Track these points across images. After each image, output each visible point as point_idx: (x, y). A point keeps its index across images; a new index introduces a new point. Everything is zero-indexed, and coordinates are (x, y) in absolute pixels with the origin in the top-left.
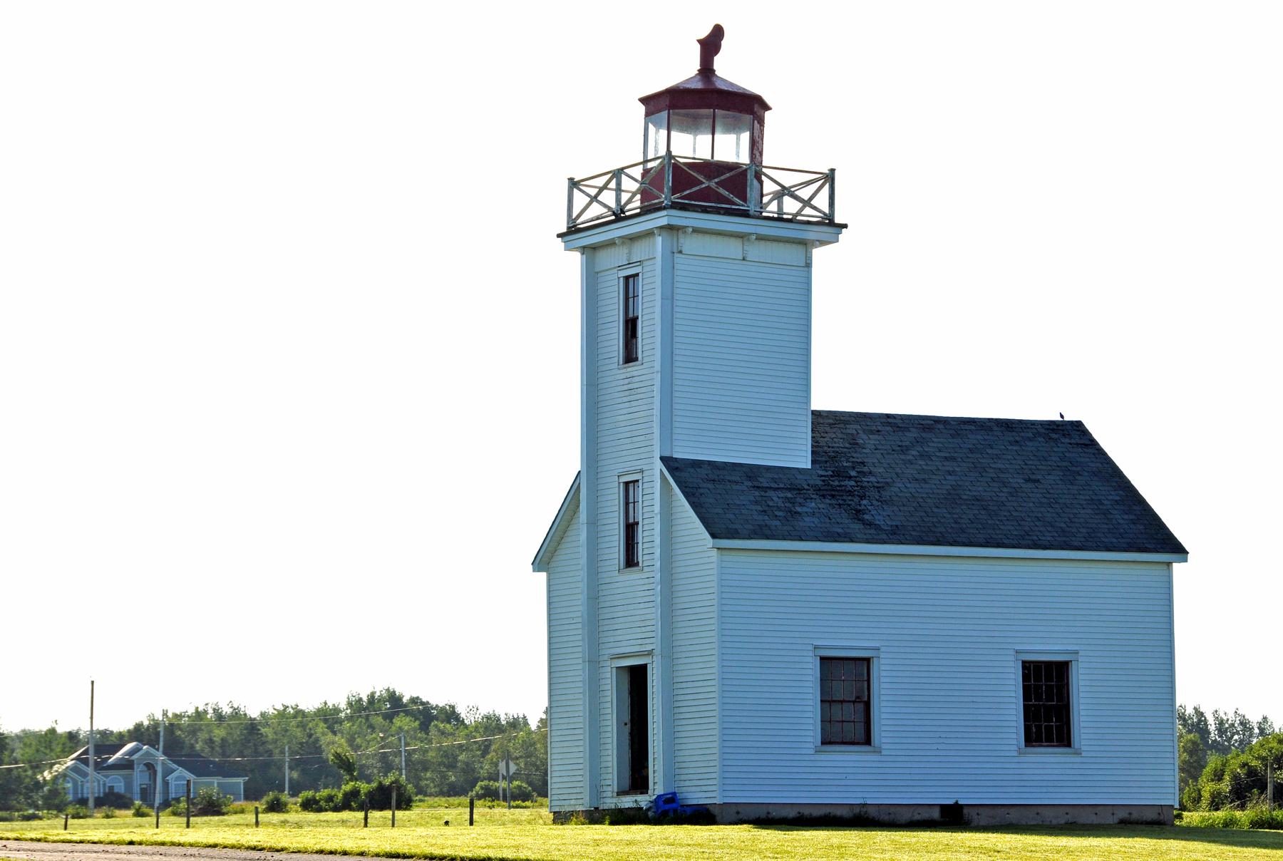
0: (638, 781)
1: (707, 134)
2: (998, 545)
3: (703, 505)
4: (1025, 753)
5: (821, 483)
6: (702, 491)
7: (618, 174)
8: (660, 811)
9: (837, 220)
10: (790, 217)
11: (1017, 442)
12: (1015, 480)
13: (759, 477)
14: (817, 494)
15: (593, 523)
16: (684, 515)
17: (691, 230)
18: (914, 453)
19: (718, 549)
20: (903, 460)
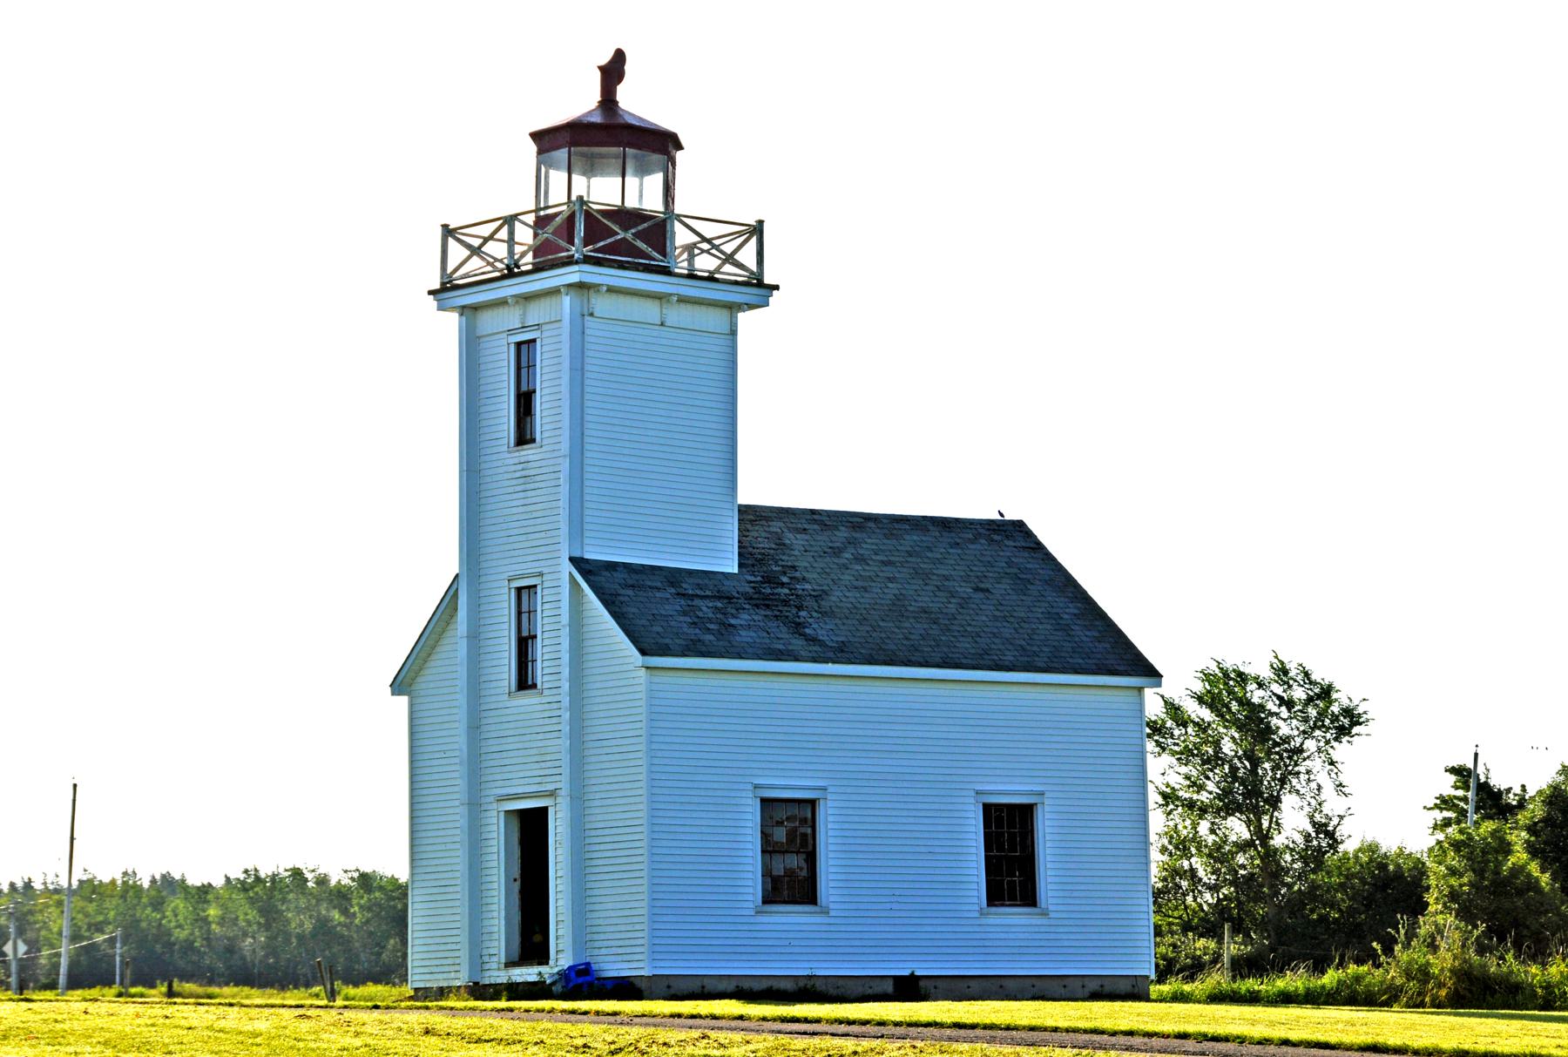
0: (533, 946)
1: (609, 174)
2: (1076, 672)
3: (625, 615)
4: (988, 914)
5: (751, 591)
6: (622, 598)
7: (510, 220)
8: (571, 985)
9: (767, 281)
10: (706, 274)
11: (958, 544)
12: (963, 589)
13: (682, 582)
14: (750, 604)
15: (474, 637)
16: (603, 627)
17: (605, 288)
18: (847, 555)
19: (647, 668)
20: (837, 564)
